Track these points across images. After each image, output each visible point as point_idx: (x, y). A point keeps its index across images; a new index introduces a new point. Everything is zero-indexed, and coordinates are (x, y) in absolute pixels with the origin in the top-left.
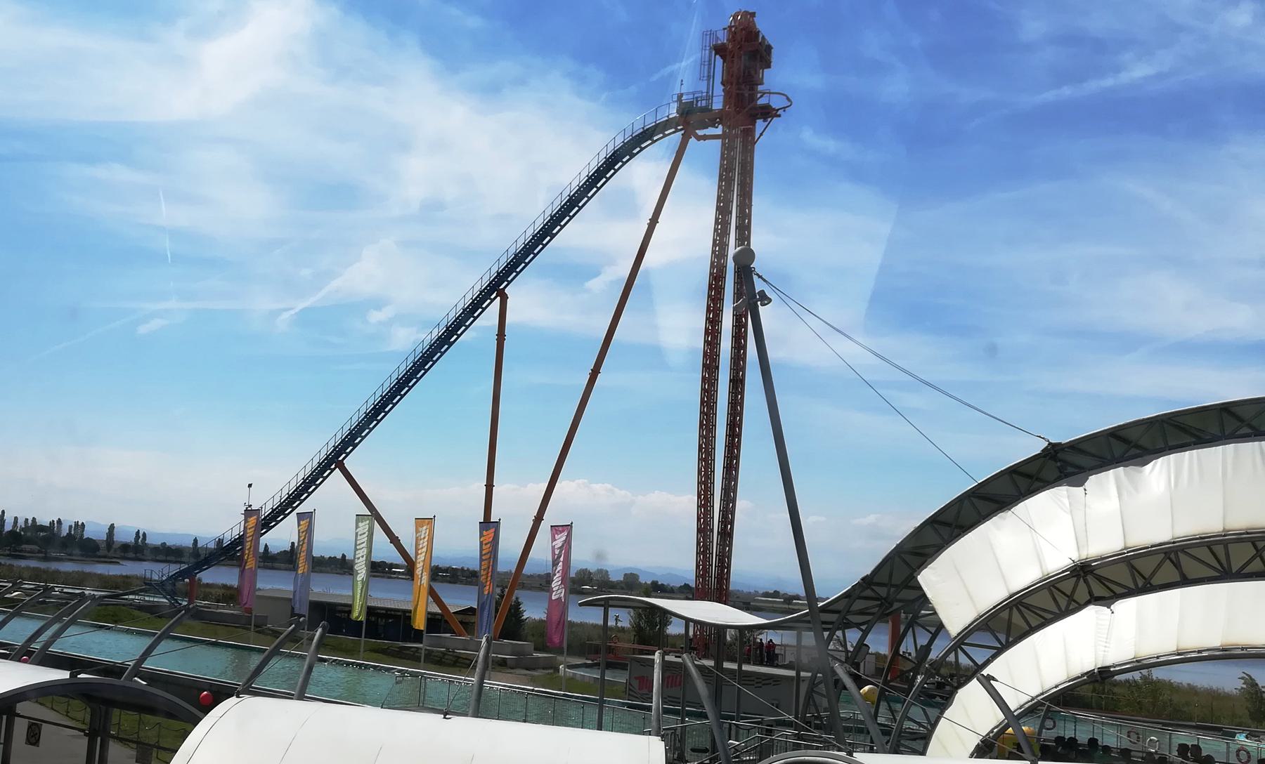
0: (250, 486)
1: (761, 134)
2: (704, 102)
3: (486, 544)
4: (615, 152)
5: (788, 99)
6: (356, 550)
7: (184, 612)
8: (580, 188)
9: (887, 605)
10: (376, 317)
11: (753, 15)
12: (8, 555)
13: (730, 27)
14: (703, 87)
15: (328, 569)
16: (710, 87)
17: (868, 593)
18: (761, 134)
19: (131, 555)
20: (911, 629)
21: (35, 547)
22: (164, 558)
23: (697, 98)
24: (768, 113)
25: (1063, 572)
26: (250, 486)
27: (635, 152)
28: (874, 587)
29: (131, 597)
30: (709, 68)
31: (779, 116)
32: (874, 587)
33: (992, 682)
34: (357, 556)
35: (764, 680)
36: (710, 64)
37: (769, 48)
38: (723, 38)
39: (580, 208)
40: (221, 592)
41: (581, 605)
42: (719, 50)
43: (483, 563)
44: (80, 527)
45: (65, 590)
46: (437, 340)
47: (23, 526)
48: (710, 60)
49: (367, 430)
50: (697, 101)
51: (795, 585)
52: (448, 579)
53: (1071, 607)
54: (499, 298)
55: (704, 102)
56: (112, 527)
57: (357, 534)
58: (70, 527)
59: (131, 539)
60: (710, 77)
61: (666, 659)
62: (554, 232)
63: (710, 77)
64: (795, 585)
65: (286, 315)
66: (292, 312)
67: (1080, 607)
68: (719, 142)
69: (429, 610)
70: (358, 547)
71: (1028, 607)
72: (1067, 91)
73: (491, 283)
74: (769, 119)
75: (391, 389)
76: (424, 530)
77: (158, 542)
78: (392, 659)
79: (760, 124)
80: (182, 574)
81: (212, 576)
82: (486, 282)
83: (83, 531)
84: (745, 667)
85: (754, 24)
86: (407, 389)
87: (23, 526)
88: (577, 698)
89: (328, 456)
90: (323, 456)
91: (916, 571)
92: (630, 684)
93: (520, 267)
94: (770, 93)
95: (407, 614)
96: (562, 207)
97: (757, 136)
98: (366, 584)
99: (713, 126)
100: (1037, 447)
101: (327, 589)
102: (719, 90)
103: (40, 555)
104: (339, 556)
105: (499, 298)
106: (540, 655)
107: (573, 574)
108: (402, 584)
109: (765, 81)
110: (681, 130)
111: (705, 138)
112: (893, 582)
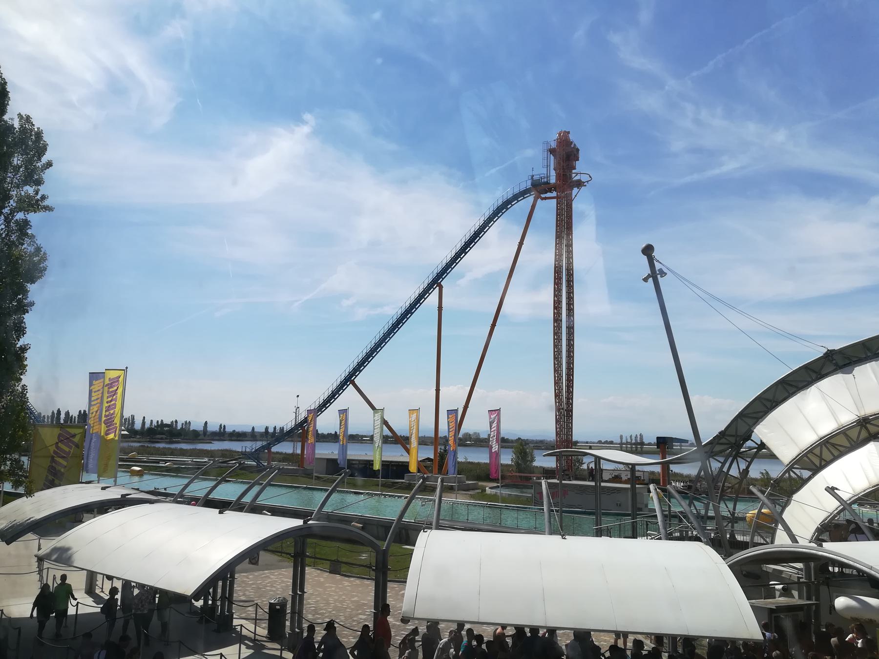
0: (298, 396)
1: (576, 196)
2: (545, 179)
3: (451, 423)
4: (498, 207)
5: (590, 177)
6: (374, 429)
7: (343, 474)
8: (480, 227)
9: (736, 447)
10: (346, 303)
11: (569, 133)
12: (149, 441)
14: (544, 171)
15: (327, 440)
16: (548, 171)
18: (576, 196)
19: (217, 438)
20: (735, 460)
21: (164, 436)
22: (236, 439)
23: (541, 177)
24: (579, 184)
25: (852, 423)
26: (298, 396)
27: (509, 207)
28: (727, 438)
30: (547, 161)
31: (585, 186)
32: (727, 438)
33: (835, 491)
34: (450, 436)
35: (611, 491)
36: (548, 159)
37: (578, 150)
38: (554, 145)
39: (480, 238)
40: (281, 456)
41: (544, 456)
42: (552, 151)
43: (450, 433)
44: (188, 424)
45: (194, 460)
46: (405, 311)
47: (156, 425)
48: (548, 157)
49: (367, 362)
50: (542, 179)
52: (394, 442)
54: (438, 287)
55: (545, 179)
56: (206, 423)
57: (374, 420)
58: (183, 424)
59: (217, 429)
60: (548, 166)
61: (602, 485)
62: (467, 251)
63: (548, 166)
66: (300, 302)
69: (383, 460)
70: (375, 428)
71: (833, 445)
72: (696, 177)
73: (433, 279)
75: (380, 339)
80: (263, 447)
81: (285, 448)
82: (430, 279)
83: (190, 426)
84: (563, 482)
86: (389, 338)
87: (156, 425)
88: (513, 507)
89: (346, 378)
91: (752, 427)
92: (535, 497)
93: (449, 270)
94: (581, 173)
95: (371, 462)
96: (471, 237)
99: (551, 192)
100: (819, 353)
101: (356, 453)
102: (553, 173)
103: (167, 440)
104: (333, 433)
105: (438, 287)
106: (470, 482)
107: (460, 436)
108: (367, 446)
109: (576, 168)
110: (533, 194)
111: (545, 198)
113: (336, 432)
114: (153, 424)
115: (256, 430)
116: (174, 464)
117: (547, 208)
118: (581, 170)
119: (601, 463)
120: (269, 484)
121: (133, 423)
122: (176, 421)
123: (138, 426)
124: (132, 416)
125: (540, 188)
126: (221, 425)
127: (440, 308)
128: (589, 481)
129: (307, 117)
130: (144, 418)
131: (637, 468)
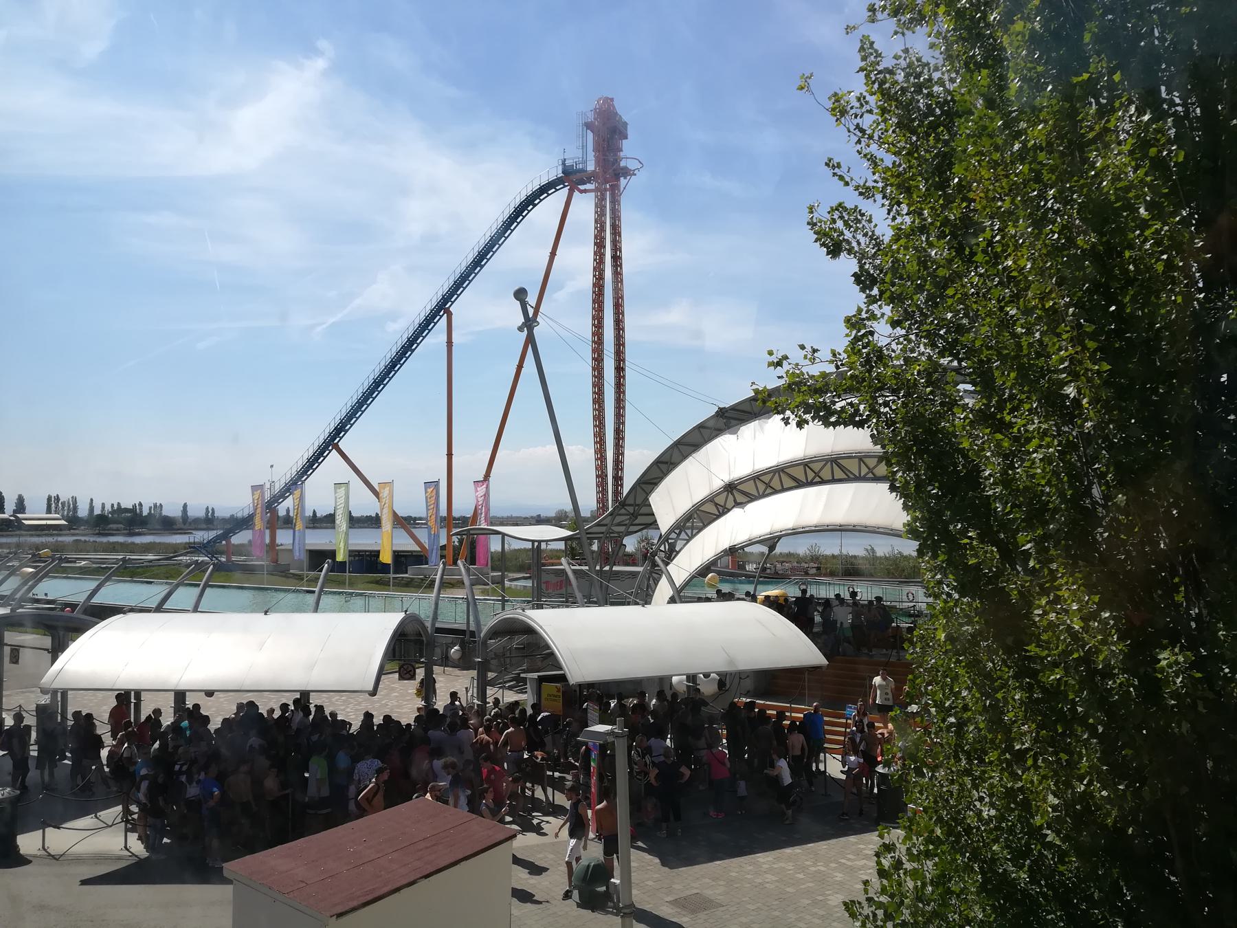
0: (272, 466)
12: (97, 534)
13: (595, 109)
15: (366, 525)
16: (585, 152)
17: (623, 511)
24: (627, 173)
26: (272, 466)
29: (179, 558)
42: (588, 126)
51: (568, 506)
53: (723, 511)
56: (185, 506)
57: (336, 497)
58: (150, 508)
59: (202, 514)
60: (584, 147)
64: (568, 506)
65: (319, 329)
66: (324, 326)
67: (729, 510)
68: (593, 194)
74: (628, 177)
76: (342, 491)
77: (227, 515)
78: (382, 587)
79: (623, 181)
80: (218, 538)
84: (615, 568)
85: (614, 107)
90: (322, 440)
97: (622, 189)
98: (347, 534)
99: (590, 183)
100: (713, 411)
102: (591, 156)
103: (125, 532)
104: (374, 515)
111: (585, 191)
112: (637, 503)
113: (377, 514)
114: (106, 509)
115: (318, 515)
116: (94, 563)
117: (584, 207)
118: (630, 150)
119: (506, 542)
120: (206, 586)
121: (75, 508)
122: (140, 504)
123: (83, 512)
124: (73, 497)
125: (571, 178)
126: (207, 508)
127: (450, 343)
128: (619, 565)
129: (323, 44)
130: (92, 500)
131: (543, 546)
